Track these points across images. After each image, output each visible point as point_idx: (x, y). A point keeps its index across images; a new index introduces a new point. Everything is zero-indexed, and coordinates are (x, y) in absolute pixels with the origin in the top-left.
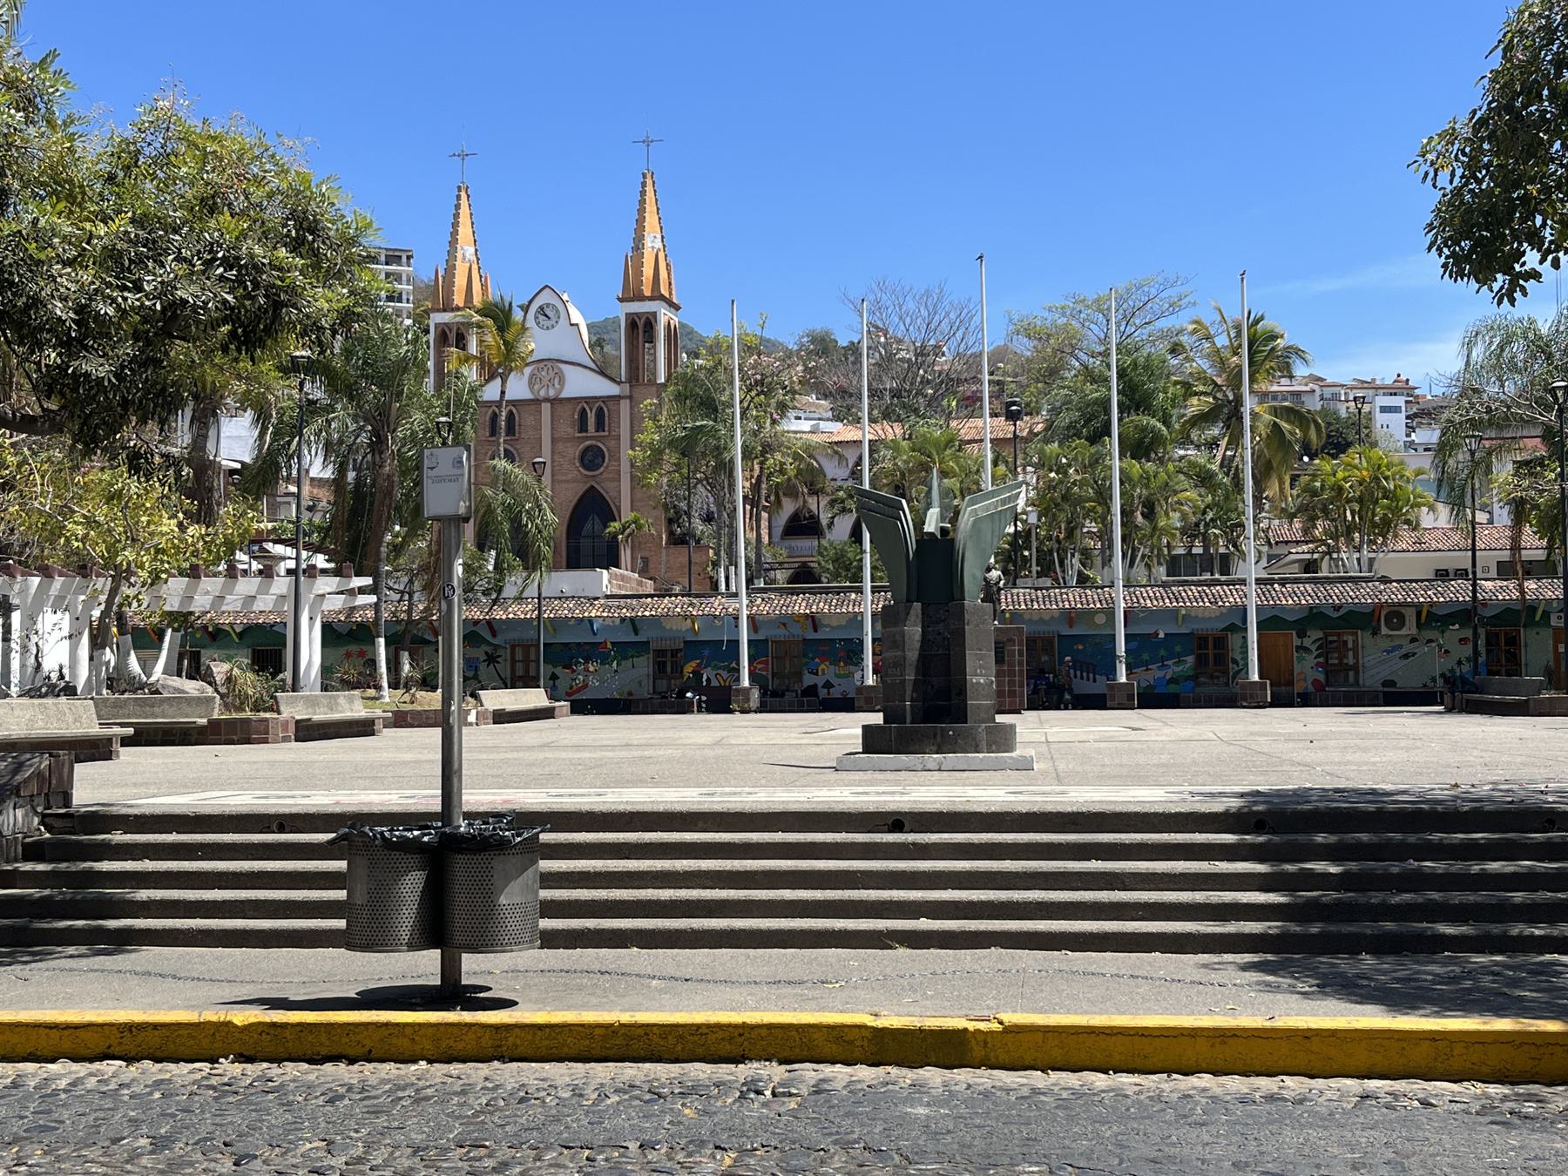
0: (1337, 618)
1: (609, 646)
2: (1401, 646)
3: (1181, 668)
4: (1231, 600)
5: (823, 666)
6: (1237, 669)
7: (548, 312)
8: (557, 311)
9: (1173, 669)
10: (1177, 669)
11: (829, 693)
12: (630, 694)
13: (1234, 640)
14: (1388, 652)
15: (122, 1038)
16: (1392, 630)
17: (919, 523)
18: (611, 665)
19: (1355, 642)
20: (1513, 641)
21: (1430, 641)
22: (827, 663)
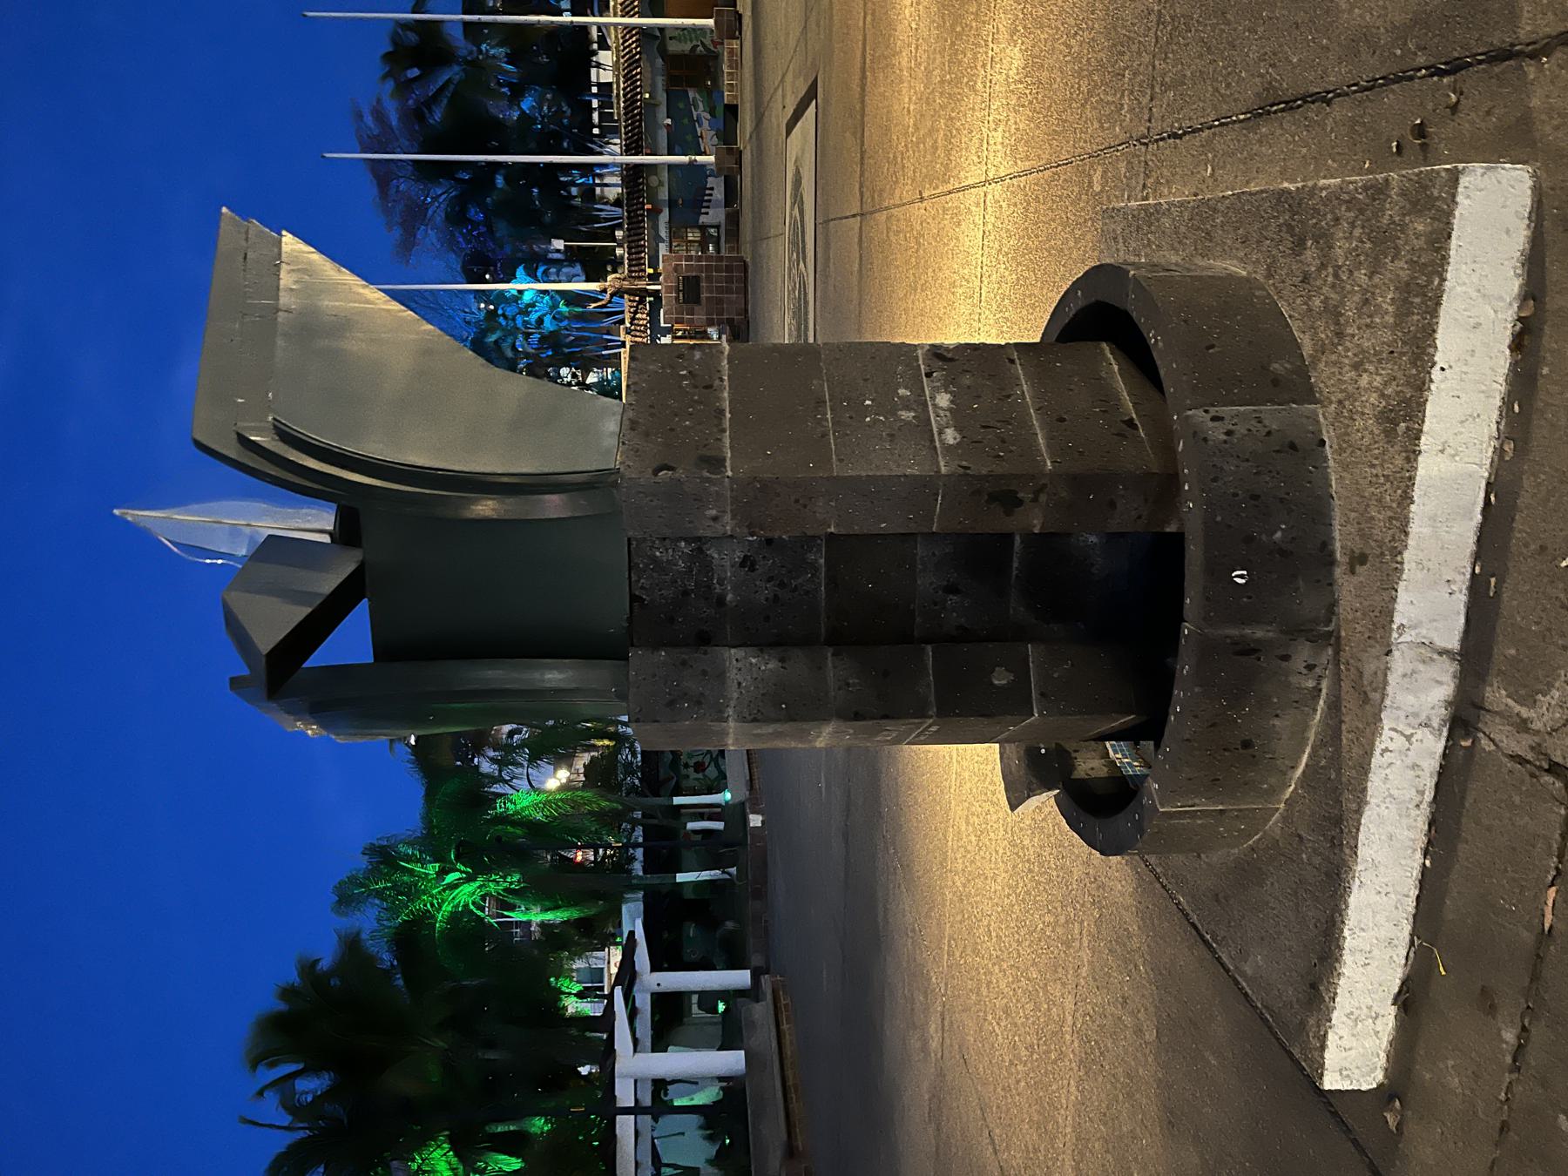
3: (701, 105)
4: (634, 46)
6: (700, 48)
9: (701, 112)
15: (1429, 570)
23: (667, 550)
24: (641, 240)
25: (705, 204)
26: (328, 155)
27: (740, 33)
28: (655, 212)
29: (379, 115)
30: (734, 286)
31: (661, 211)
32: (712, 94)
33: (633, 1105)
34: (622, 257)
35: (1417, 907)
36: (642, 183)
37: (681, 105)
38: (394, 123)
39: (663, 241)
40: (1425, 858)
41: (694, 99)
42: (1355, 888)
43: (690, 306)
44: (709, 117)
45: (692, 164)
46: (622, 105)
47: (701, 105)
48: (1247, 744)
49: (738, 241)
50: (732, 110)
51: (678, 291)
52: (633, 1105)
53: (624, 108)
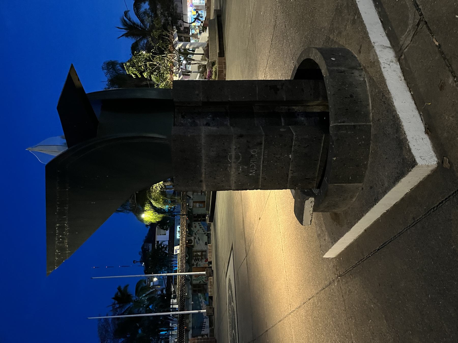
9: (202, 299)
21: (195, 234)
23: (185, 121)
24: (183, 339)
25: (203, 327)
27: (213, 275)
28: (187, 331)
35: (416, 106)
40: (411, 93)
41: (200, 296)
42: (394, 100)
44: (204, 300)
46: (179, 299)
47: (202, 297)
48: (351, 96)
50: (211, 298)
53: (180, 300)
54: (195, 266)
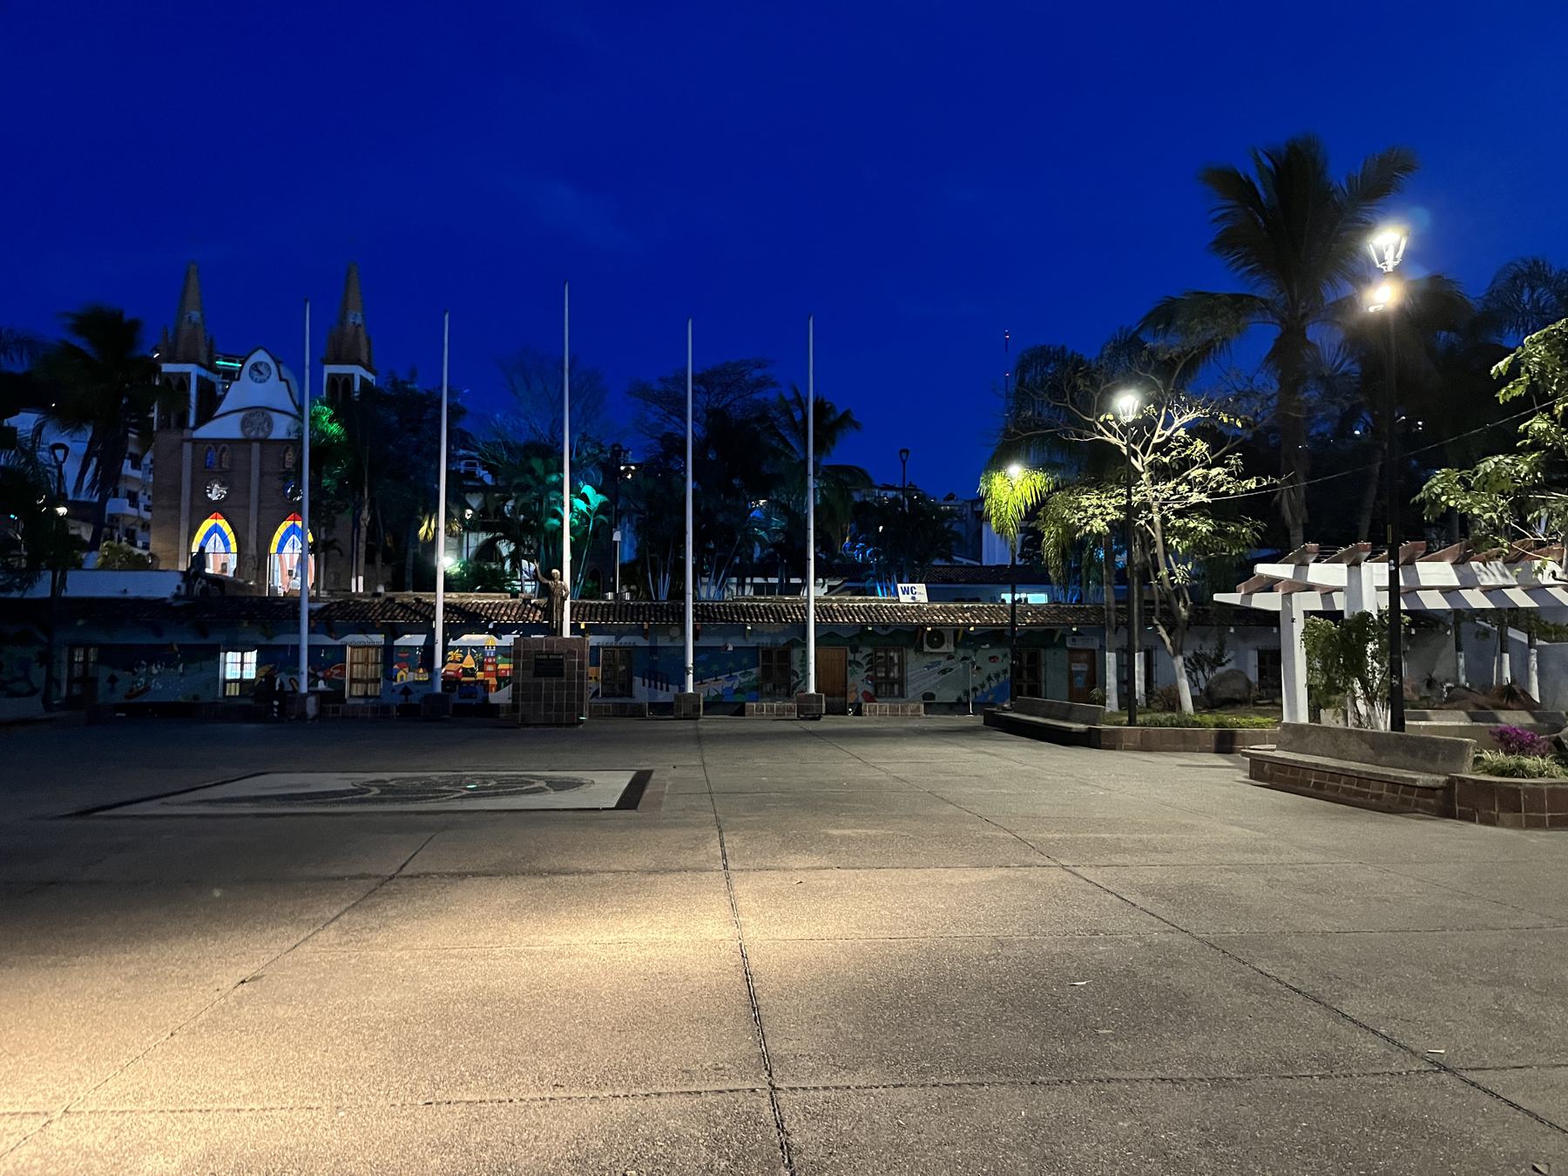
0: (886, 636)
1: (176, 648)
2: (939, 663)
3: (747, 679)
5: (401, 673)
6: (796, 680)
7: (261, 368)
8: (269, 369)
9: (740, 680)
10: (743, 680)
11: (407, 700)
12: (196, 698)
13: (796, 654)
14: (929, 667)
16: (933, 648)
17: (132, 432)
18: (177, 668)
19: (901, 659)
20: (1034, 658)
21: (965, 658)
22: (407, 669)
24: (602, 618)
26: (447, 317)
27: (802, 719)
29: (761, 384)
30: (553, 713)
31: (646, 638)
32: (757, 691)
33: (48, 594)
34: (605, 598)
36: (668, 621)
37: (745, 661)
38: (756, 396)
39: (617, 640)
43: (533, 666)
44: (735, 687)
45: (686, 670)
49: (615, 716)
50: (740, 711)
51: (548, 654)
52: (48, 594)
53: (741, 606)
54: (851, 657)
